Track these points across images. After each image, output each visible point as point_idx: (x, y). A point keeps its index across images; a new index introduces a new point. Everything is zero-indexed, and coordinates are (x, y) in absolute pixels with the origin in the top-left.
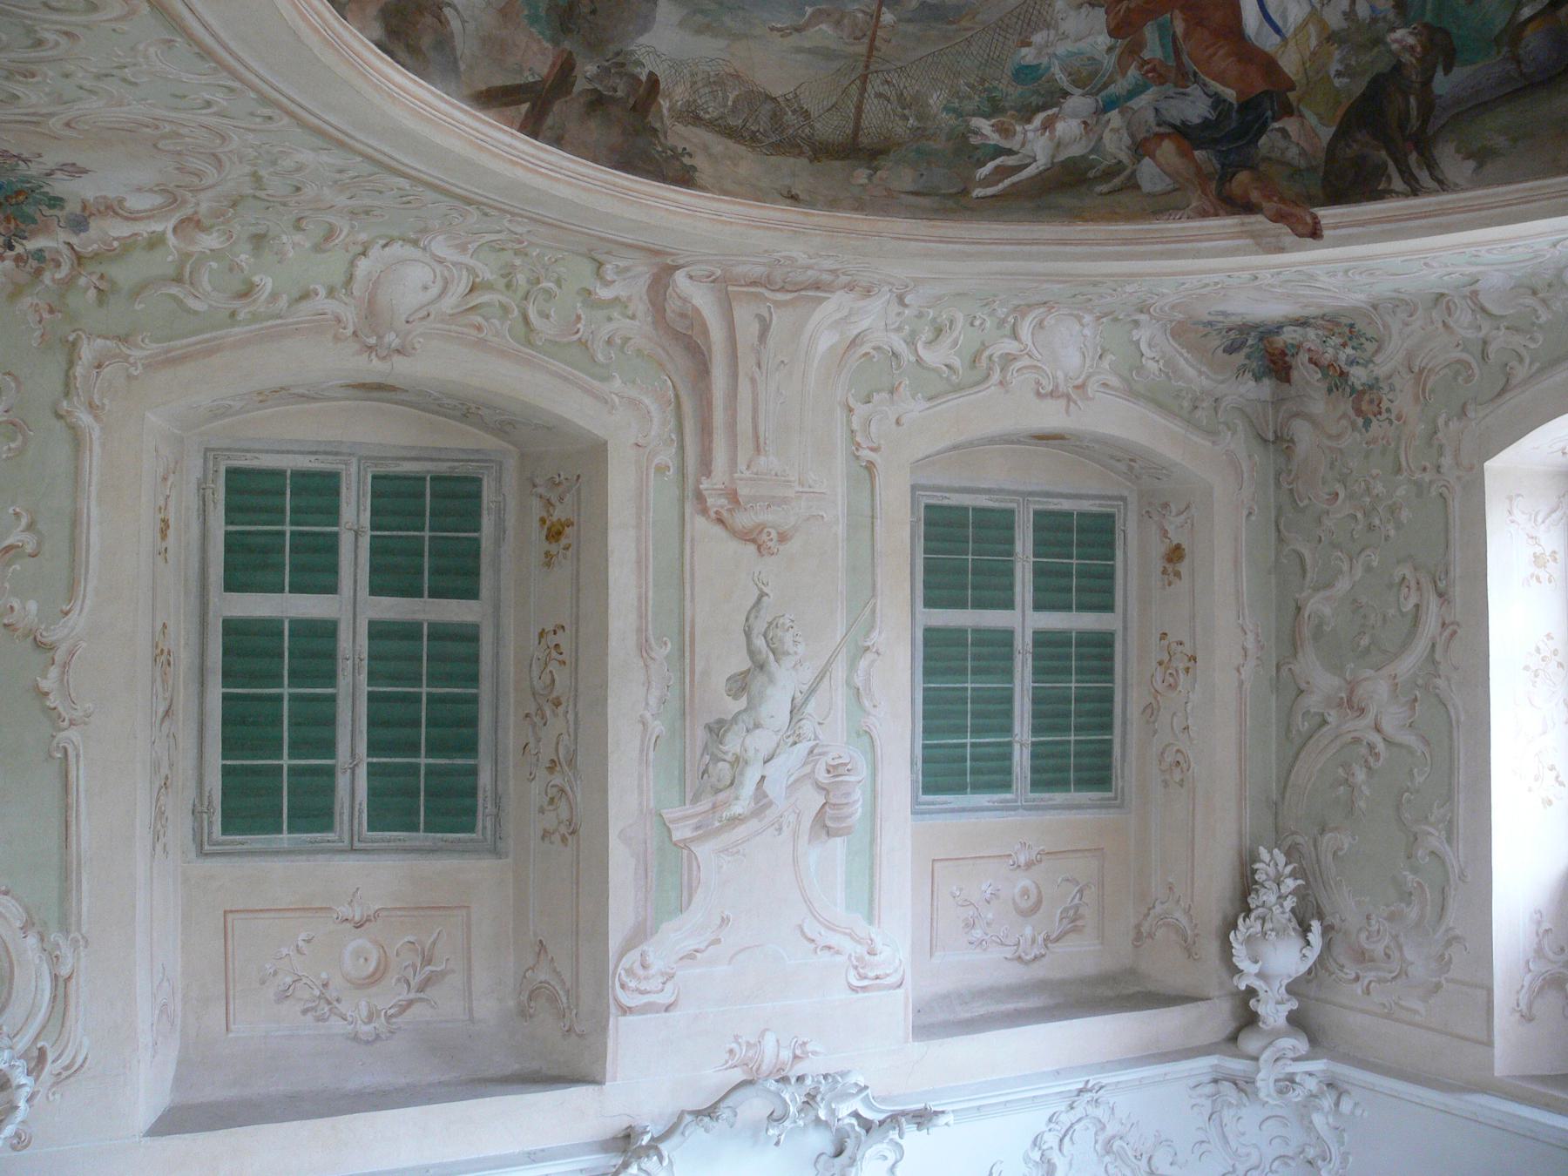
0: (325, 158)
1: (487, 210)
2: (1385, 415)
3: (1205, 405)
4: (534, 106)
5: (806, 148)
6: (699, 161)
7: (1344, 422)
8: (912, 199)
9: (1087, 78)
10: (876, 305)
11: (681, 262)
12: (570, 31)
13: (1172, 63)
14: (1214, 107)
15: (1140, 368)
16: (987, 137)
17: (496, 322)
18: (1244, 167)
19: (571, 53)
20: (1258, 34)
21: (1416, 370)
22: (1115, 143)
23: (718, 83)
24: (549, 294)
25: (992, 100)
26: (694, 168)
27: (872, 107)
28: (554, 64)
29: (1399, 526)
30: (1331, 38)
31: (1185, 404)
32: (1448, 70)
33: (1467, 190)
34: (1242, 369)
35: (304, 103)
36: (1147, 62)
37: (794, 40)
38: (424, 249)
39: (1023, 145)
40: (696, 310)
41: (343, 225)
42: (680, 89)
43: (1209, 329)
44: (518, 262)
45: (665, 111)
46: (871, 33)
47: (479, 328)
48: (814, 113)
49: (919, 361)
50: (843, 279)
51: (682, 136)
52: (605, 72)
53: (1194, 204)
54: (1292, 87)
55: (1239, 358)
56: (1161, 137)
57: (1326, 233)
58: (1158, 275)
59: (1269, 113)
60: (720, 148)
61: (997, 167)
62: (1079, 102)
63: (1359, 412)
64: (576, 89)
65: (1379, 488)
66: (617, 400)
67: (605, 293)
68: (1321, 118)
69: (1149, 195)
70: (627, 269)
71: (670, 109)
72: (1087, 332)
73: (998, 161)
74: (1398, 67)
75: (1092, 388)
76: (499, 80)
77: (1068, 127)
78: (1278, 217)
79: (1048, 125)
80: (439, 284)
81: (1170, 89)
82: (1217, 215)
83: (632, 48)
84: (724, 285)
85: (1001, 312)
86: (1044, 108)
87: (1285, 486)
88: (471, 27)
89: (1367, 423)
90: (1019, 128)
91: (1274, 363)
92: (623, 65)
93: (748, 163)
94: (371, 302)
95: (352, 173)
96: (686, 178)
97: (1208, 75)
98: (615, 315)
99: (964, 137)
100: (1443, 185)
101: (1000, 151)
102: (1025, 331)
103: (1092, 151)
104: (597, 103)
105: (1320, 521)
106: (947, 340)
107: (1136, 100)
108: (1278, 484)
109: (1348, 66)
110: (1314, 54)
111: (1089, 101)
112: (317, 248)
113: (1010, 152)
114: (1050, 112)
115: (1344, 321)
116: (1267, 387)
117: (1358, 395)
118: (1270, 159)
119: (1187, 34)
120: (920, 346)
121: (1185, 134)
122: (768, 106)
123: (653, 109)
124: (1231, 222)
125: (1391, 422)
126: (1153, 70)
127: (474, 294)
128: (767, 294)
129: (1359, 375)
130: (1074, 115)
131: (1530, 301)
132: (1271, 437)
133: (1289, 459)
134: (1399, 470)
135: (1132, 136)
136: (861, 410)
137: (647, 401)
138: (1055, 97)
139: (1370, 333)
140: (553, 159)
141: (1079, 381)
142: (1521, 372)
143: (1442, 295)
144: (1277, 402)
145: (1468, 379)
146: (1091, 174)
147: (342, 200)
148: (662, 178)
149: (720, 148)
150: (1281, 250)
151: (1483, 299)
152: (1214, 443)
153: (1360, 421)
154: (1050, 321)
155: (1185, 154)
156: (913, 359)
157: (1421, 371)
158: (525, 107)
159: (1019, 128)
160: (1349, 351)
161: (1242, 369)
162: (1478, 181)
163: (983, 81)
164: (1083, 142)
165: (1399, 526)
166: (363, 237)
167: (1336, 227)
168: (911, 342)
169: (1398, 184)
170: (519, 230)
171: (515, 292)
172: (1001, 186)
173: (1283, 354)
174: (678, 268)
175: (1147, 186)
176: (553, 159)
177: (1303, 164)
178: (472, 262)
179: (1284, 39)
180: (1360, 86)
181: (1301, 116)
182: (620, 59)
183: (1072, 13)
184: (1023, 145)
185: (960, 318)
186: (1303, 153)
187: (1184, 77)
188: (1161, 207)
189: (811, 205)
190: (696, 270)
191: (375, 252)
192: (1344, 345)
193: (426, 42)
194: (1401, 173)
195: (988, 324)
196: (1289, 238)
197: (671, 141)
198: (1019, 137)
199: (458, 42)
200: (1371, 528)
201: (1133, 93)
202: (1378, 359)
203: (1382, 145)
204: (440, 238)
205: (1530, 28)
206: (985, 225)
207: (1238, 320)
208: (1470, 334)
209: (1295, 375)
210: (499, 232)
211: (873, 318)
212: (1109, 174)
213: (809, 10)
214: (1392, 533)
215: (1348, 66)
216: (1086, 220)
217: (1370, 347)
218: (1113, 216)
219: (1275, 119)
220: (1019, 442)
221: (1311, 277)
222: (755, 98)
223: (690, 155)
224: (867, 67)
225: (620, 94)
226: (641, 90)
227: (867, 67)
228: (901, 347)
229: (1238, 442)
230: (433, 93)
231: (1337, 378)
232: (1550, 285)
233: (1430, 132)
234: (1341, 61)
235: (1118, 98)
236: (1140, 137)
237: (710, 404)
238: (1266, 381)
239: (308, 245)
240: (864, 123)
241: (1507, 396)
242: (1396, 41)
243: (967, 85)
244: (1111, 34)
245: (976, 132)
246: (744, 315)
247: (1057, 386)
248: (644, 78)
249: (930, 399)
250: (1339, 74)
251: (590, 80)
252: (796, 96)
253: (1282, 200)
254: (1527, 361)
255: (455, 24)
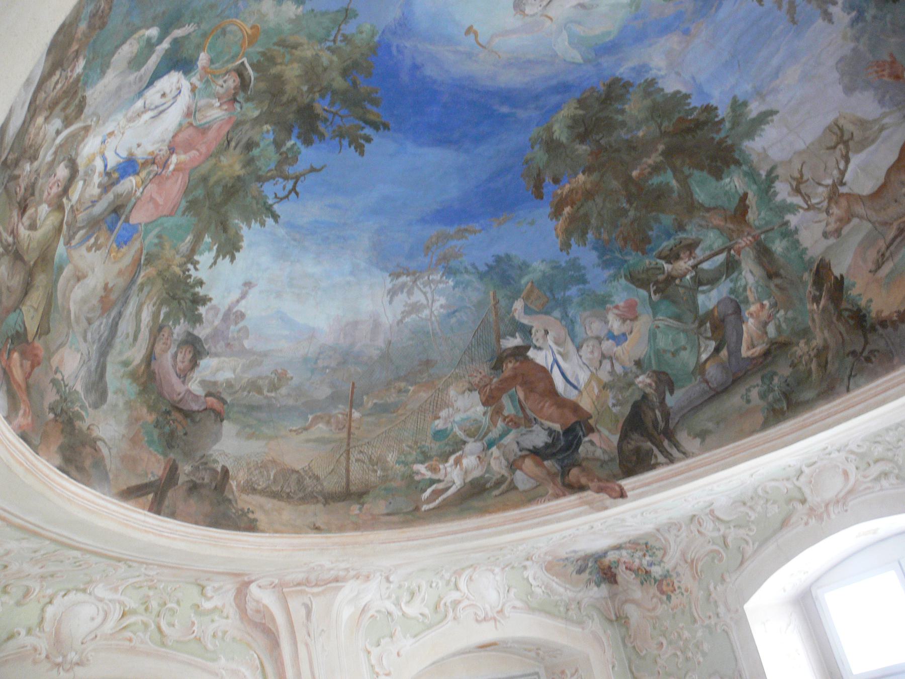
0: (25, 544)
1: (130, 563)
2: (678, 591)
3: (573, 607)
4: (156, 495)
5: (320, 498)
6: (259, 515)
7: (655, 600)
8: (388, 518)
9: (475, 432)
10: (373, 585)
11: (253, 578)
12: (173, 447)
13: (521, 415)
14: (550, 435)
15: (532, 593)
16: (423, 475)
17: (141, 634)
18: (574, 465)
19: (174, 460)
20: (565, 390)
21: (689, 561)
22: (498, 465)
23: (263, 466)
24: (173, 612)
25: (423, 453)
26: (255, 520)
27: (355, 467)
28: (165, 469)
29: (704, 654)
30: (605, 387)
31: (562, 609)
32: (672, 393)
33: (699, 454)
34: (589, 581)
35: (12, 511)
36: (508, 417)
37: (304, 435)
38: (90, 594)
39: (446, 476)
40: (265, 607)
41: (36, 586)
42: (241, 474)
43: (566, 562)
44: (151, 593)
45: (234, 488)
46: (347, 425)
47: (130, 640)
48: (322, 477)
49: (404, 614)
50: (352, 573)
51: (246, 501)
52: (196, 469)
53: (550, 492)
54: (591, 417)
55: (586, 576)
56: (524, 457)
57: (629, 494)
58: (538, 536)
59: (581, 433)
60: (270, 505)
61: (433, 491)
62: (473, 446)
63: (662, 592)
64: (180, 482)
65: (686, 634)
66: (224, 672)
67: (207, 605)
68: (610, 431)
69: (525, 491)
70: (220, 588)
71: (238, 486)
72: (498, 578)
73: (434, 487)
74: (645, 397)
75: (507, 610)
76: (134, 482)
77: (469, 461)
78: (600, 490)
79: (458, 462)
80: (102, 614)
81: (523, 429)
82: (564, 495)
83: (211, 452)
84: (281, 588)
85: (447, 576)
86: (454, 452)
87: (629, 645)
88: (114, 451)
89: (669, 598)
90: (441, 466)
91: (605, 574)
92: (206, 463)
93: (288, 512)
94: (57, 633)
95: (42, 552)
96: (251, 527)
97: (541, 418)
98: (216, 618)
99: (411, 476)
100: (686, 455)
101: (432, 482)
102: (462, 584)
103: (487, 471)
104: (194, 488)
105: (656, 662)
106: (418, 599)
107: (505, 439)
108: (625, 645)
109: (618, 400)
110: (598, 397)
111: (479, 444)
112: (18, 604)
113: (439, 481)
114: (458, 454)
115: (642, 542)
116: (604, 589)
117: (659, 582)
118: (587, 459)
119: (526, 398)
120: (403, 605)
121: (536, 453)
122: (295, 476)
123: (227, 487)
124: (573, 498)
125: (682, 594)
126: (511, 420)
127: (125, 619)
128: (307, 589)
129: (657, 571)
130: (472, 454)
131: (743, 509)
132: (614, 618)
133: (628, 629)
134: (695, 621)
135: (507, 460)
136: (375, 651)
137: (243, 670)
138: (459, 445)
139: (657, 545)
140: (170, 526)
141: (499, 608)
142: (749, 550)
143: (694, 516)
144: (613, 596)
145: (721, 560)
146: (488, 486)
147: (36, 570)
148: (237, 527)
149: (270, 505)
150: (606, 508)
151: (717, 513)
152: (583, 629)
153: (664, 598)
154: (475, 576)
155: (539, 465)
156: (400, 614)
157: (692, 561)
158: (151, 496)
159: (441, 466)
160: (648, 558)
161: (589, 581)
162: (705, 449)
163: (416, 443)
164: (480, 469)
165: (704, 654)
166: (49, 591)
167: (633, 489)
168: (397, 604)
169: (661, 458)
170: (151, 573)
171: (151, 612)
172: (437, 502)
173: (610, 568)
174: (252, 582)
175: (521, 486)
176: (170, 526)
177: (606, 458)
178: (122, 598)
179: (580, 392)
180: (627, 410)
181: (599, 431)
182: (204, 460)
183: (460, 397)
184: (446, 476)
185: (424, 585)
186: (605, 452)
187: (529, 422)
188: (531, 497)
189: (329, 531)
190: (263, 582)
191: (58, 601)
192: (644, 555)
193: (88, 463)
194: (661, 452)
195: (440, 584)
196: (609, 501)
197: (241, 505)
198: (443, 472)
199: (107, 461)
200: (687, 659)
201: (501, 437)
202: (666, 559)
203: (647, 438)
204: (101, 585)
205: (708, 365)
206: (432, 526)
207: (582, 554)
208: (716, 534)
209: (619, 579)
210: (138, 576)
211: (373, 594)
212: (498, 484)
213: (310, 417)
214: (701, 659)
215: (618, 400)
216: (490, 513)
217: (659, 554)
218: (505, 507)
219: (584, 436)
220: (470, 652)
221: (623, 520)
222: (286, 473)
223: (253, 512)
224: (348, 445)
225: (206, 481)
226: (219, 477)
227: (348, 445)
228: (392, 608)
229: (596, 625)
230: (95, 495)
231: (644, 576)
232: (752, 498)
233: (671, 426)
234: (613, 398)
235: (495, 440)
236: (511, 460)
237: (282, 664)
238: (603, 586)
239: (12, 602)
240: (352, 477)
241: (746, 564)
242: (640, 382)
243: (408, 446)
244: (484, 404)
245: (418, 473)
246: (296, 605)
247: (487, 614)
248: (219, 469)
249: (415, 636)
250: (614, 405)
251: (188, 475)
252: (310, 468)
253: (599, 480)
254: (751, 543)
255: (105, 451)
